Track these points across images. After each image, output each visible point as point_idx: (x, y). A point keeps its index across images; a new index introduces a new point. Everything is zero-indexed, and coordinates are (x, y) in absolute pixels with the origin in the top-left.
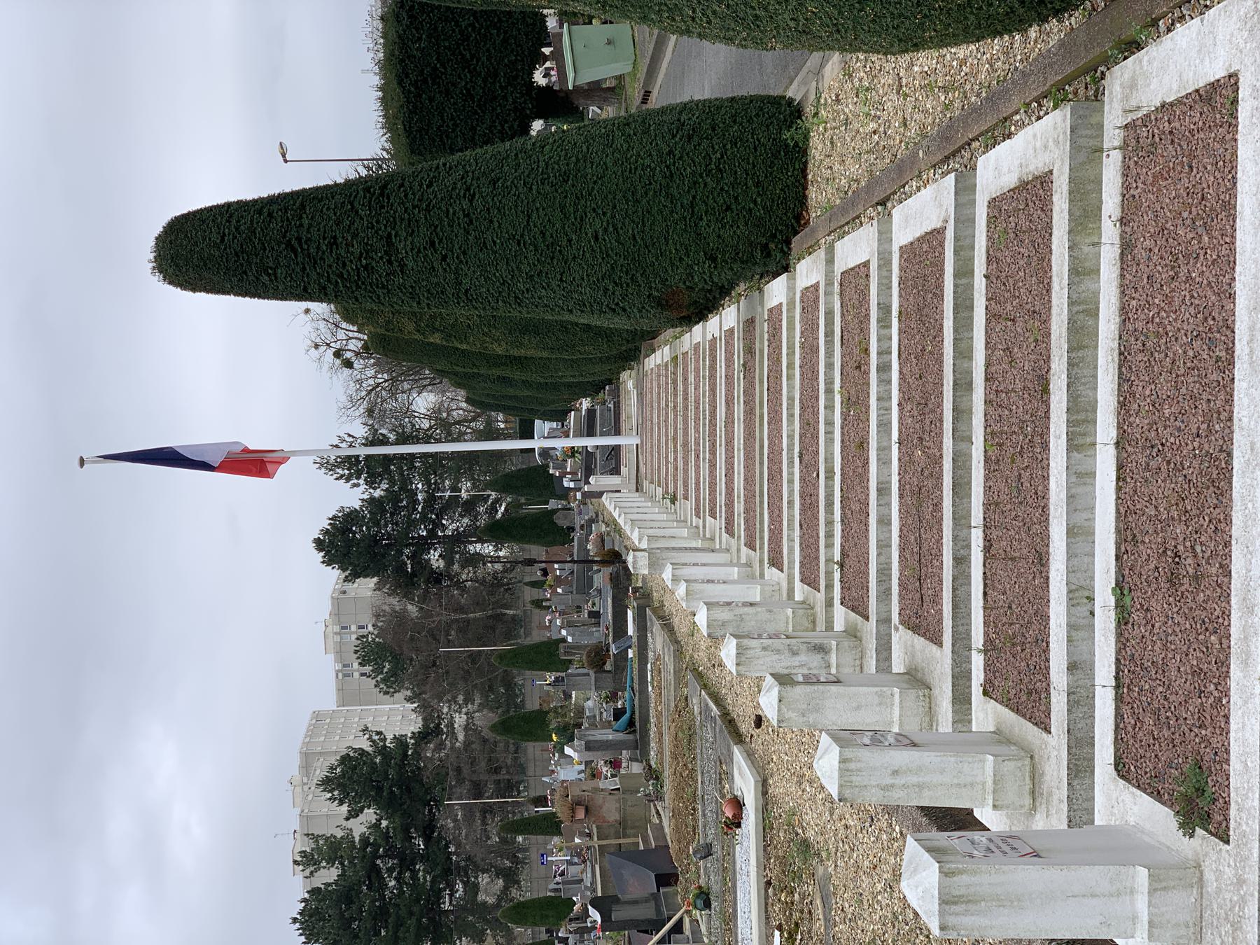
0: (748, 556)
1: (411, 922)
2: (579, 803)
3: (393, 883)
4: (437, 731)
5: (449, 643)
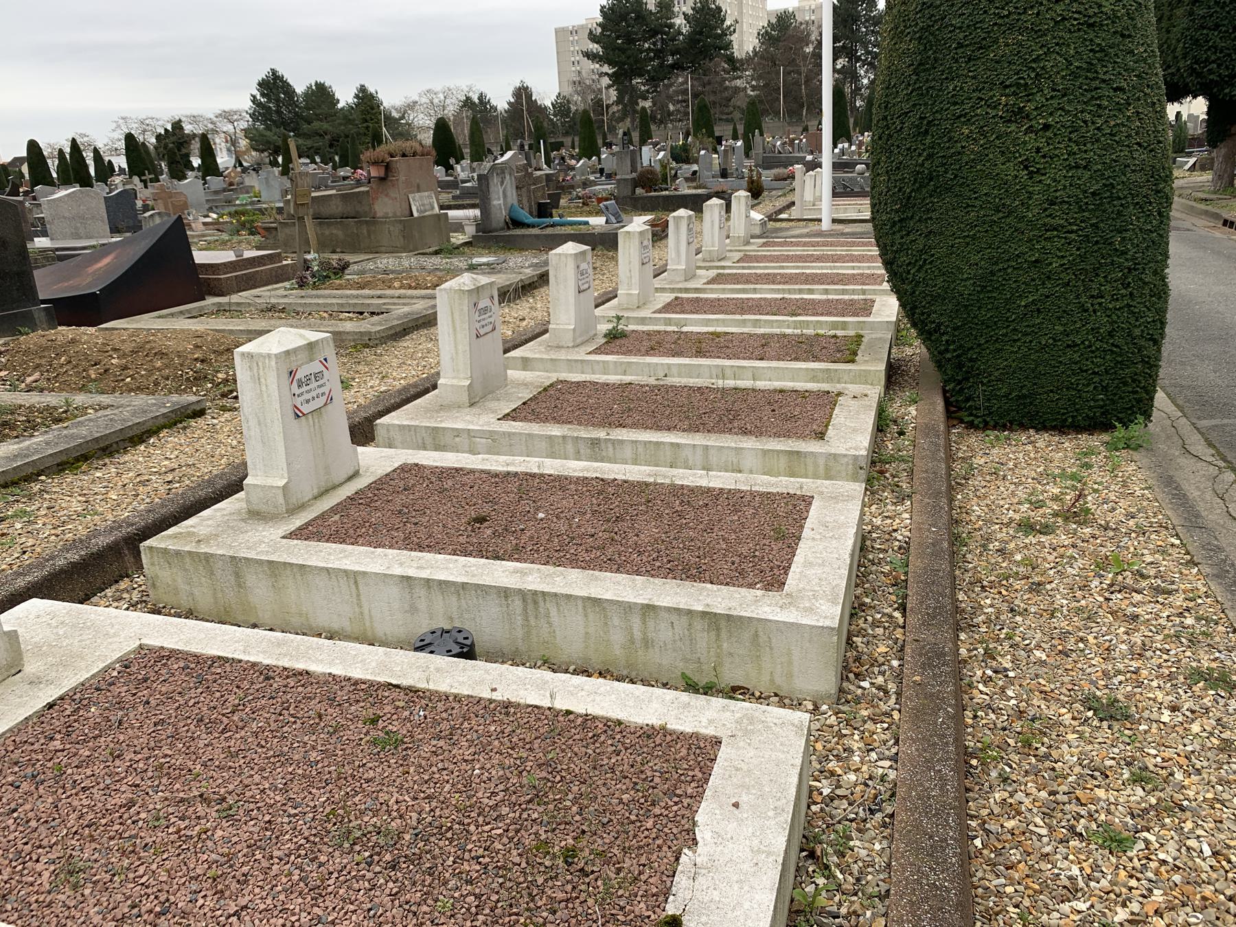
0: (700, 277)
1: (623, 58)
2: (388, 168)
3: (647, 45)
4: (735, 69)
5: (786, 73)
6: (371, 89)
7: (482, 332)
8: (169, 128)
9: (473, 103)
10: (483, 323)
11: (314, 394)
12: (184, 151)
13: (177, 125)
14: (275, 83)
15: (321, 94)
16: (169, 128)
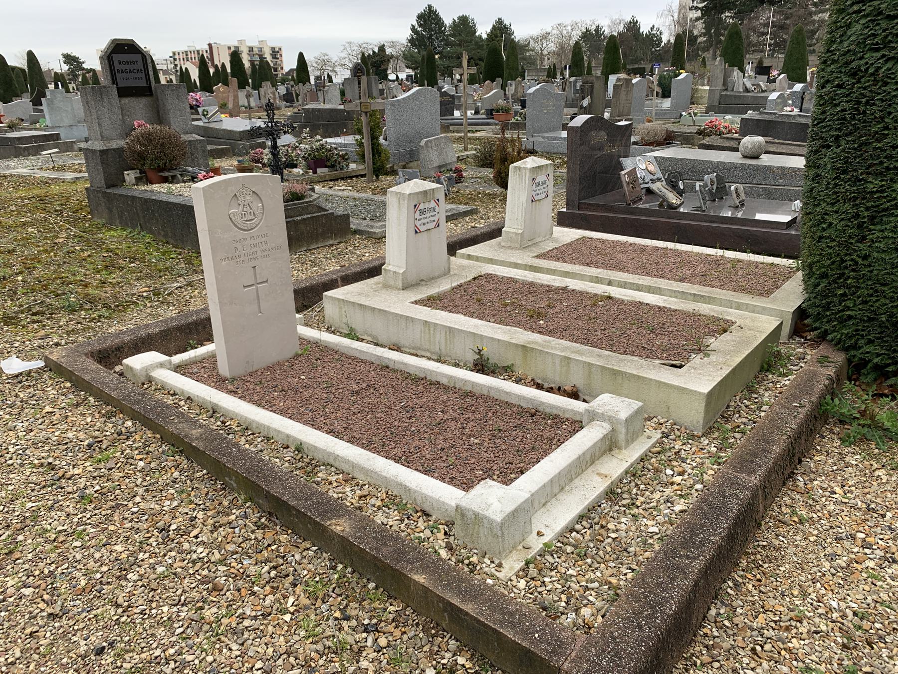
6: (507, 22)
7: (422, 228)
8: (376, 50)
9: (591, 34)
10: (538, 192)
11: (428, 220)
12: (383, 67)
13: (382, 48)
14: (430, 16)
15: (464, 25)
16: (376, 50)
